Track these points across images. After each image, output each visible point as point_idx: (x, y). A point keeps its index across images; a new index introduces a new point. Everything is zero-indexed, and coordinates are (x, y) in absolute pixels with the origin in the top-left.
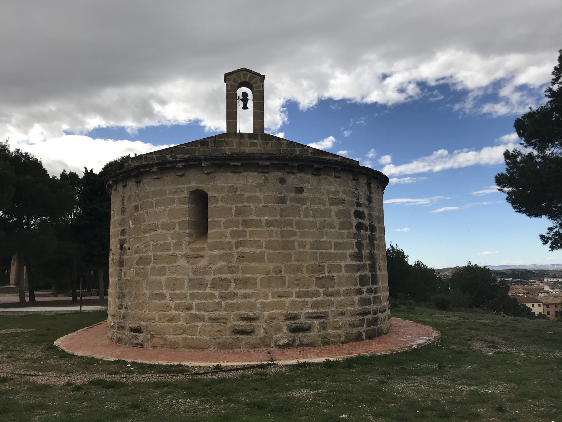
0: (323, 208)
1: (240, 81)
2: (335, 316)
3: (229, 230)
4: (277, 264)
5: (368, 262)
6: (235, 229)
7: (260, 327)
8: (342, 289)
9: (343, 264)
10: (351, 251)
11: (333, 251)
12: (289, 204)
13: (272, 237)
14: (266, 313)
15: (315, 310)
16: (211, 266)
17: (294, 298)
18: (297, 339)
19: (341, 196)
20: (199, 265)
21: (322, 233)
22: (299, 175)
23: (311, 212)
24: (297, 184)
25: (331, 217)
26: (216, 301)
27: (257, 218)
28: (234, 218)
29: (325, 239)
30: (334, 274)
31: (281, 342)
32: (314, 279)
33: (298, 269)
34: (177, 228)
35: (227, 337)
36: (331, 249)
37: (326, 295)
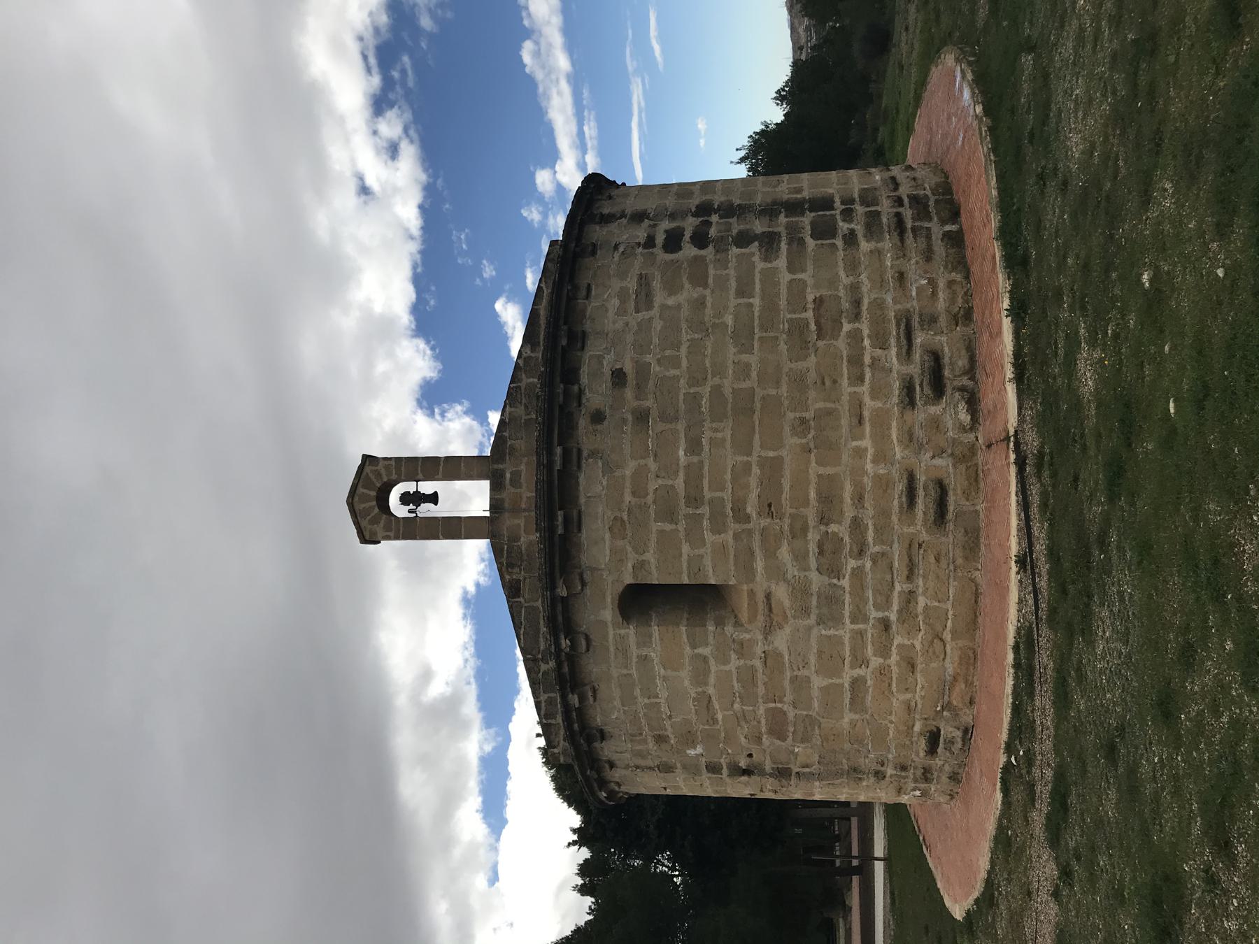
0: (658, 325)
1: (377, 510)
2: (908, 297)
3: (709, 537)
4: (787, 429)
5: (782, 219)
6: (706, 523)
7: (929, 466)
8: (845, 280)
9: (785, 277)
10: (756, 258)
11: (756, 301)
12: (649, 403)
13: (724, 440)
14: (899, 452)
15: (893, 341)
16: (789, 576)
17: (865, 389)
18: (957, 383)
19: (632, 284)
20: (787, 603)
21: (715, 326)
22: (584, 379)
23: (668, 353)
24: (605, 385)
25: (679, 307)
26: (868, 564)
27: (681, 474)
28: (682, 526)
29: (729, 319)
30: (810, 298)
31: (965, 417)
32: (820, 343)
33: (799, 381)
34: (705, 651)
35: (951, 540)
36: (751, 305)
37: (857, 317)
